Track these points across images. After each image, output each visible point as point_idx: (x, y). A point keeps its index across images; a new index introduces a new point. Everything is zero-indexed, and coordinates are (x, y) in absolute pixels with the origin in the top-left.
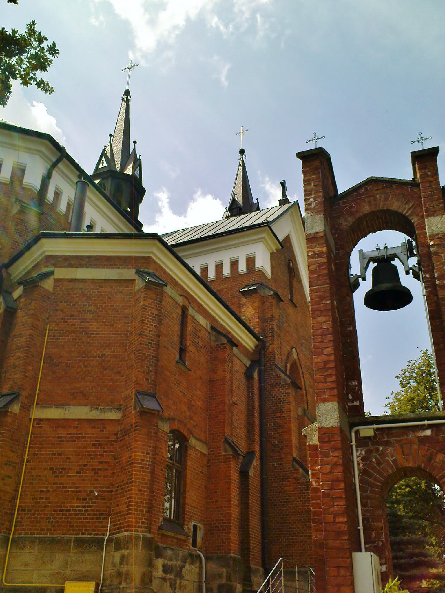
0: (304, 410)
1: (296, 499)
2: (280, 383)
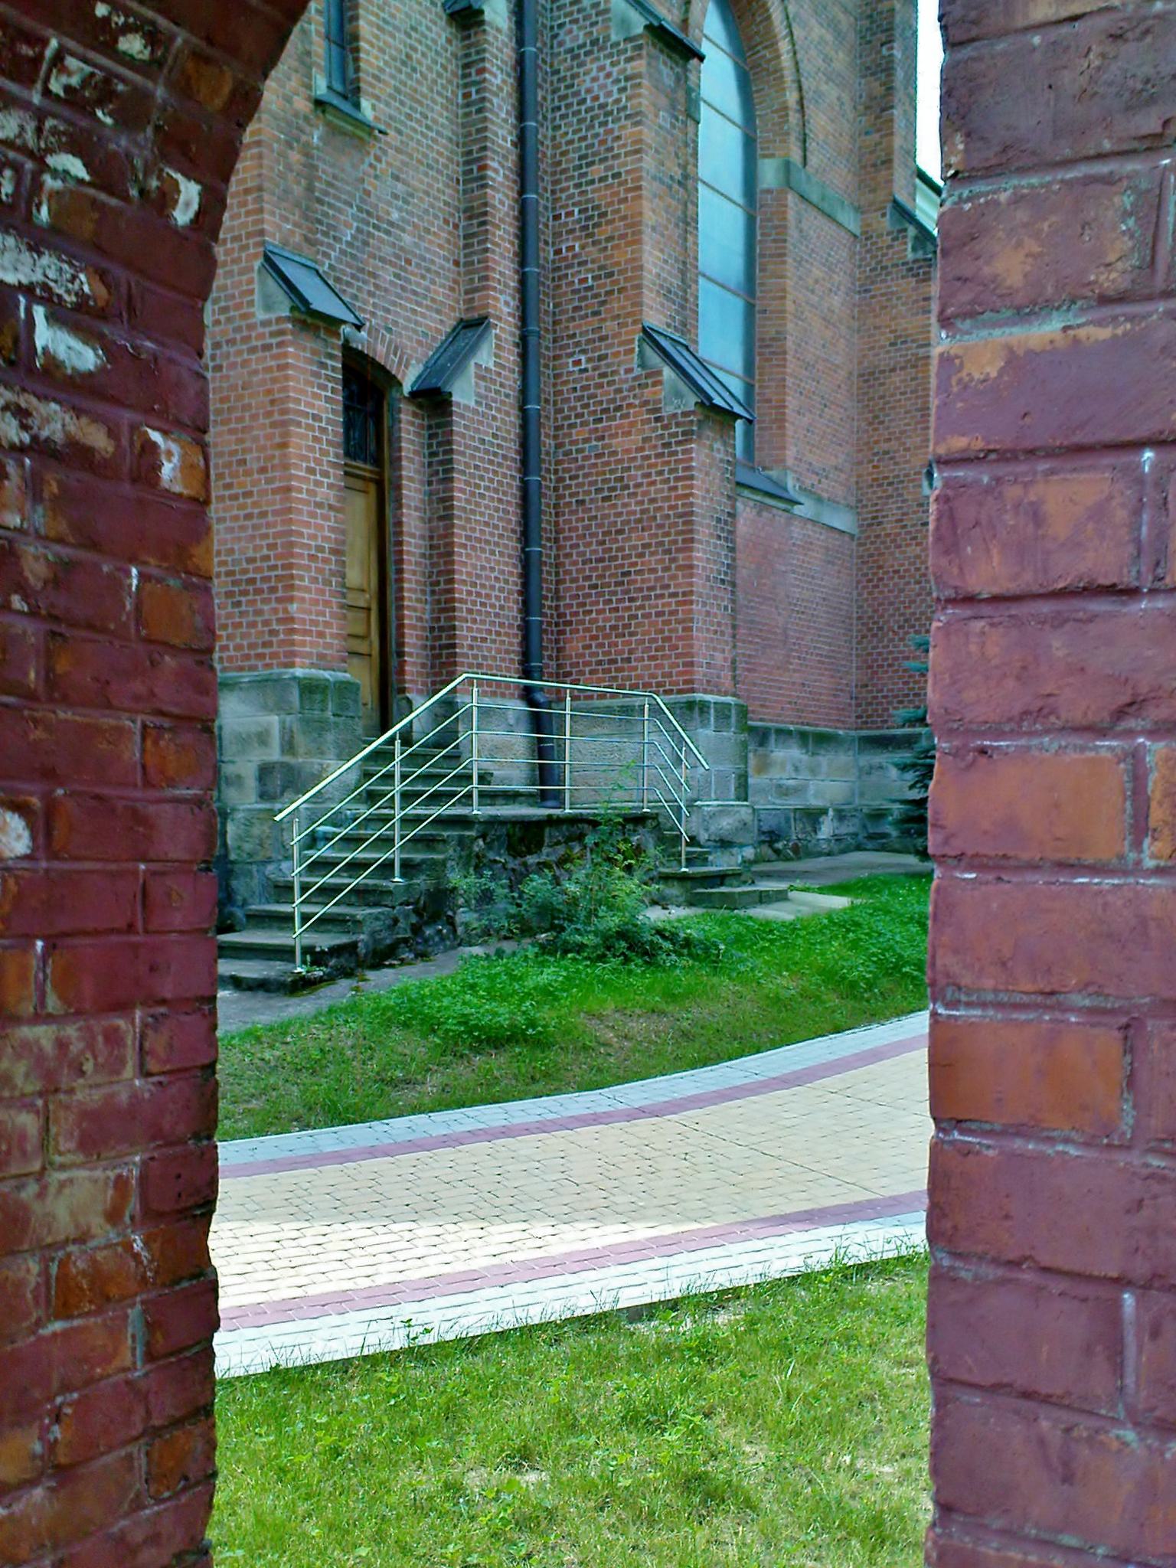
0: (787, 166)
1: (649, 475)
2: (607, 38)
